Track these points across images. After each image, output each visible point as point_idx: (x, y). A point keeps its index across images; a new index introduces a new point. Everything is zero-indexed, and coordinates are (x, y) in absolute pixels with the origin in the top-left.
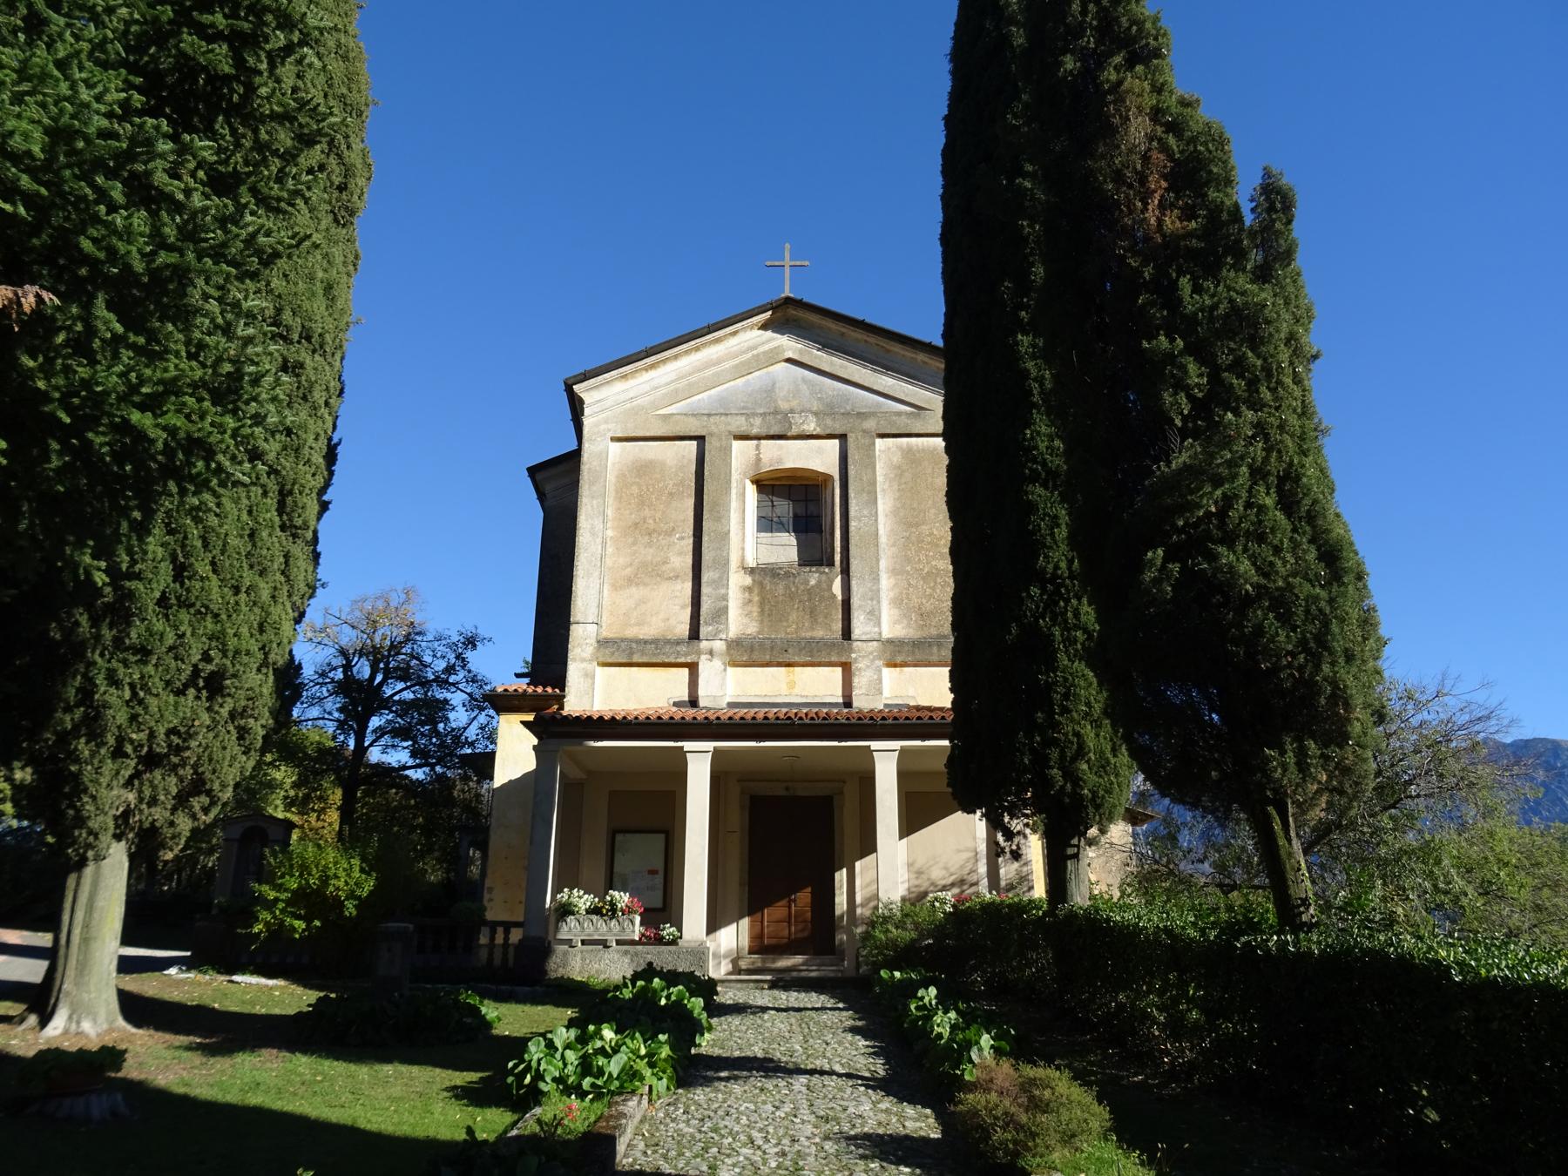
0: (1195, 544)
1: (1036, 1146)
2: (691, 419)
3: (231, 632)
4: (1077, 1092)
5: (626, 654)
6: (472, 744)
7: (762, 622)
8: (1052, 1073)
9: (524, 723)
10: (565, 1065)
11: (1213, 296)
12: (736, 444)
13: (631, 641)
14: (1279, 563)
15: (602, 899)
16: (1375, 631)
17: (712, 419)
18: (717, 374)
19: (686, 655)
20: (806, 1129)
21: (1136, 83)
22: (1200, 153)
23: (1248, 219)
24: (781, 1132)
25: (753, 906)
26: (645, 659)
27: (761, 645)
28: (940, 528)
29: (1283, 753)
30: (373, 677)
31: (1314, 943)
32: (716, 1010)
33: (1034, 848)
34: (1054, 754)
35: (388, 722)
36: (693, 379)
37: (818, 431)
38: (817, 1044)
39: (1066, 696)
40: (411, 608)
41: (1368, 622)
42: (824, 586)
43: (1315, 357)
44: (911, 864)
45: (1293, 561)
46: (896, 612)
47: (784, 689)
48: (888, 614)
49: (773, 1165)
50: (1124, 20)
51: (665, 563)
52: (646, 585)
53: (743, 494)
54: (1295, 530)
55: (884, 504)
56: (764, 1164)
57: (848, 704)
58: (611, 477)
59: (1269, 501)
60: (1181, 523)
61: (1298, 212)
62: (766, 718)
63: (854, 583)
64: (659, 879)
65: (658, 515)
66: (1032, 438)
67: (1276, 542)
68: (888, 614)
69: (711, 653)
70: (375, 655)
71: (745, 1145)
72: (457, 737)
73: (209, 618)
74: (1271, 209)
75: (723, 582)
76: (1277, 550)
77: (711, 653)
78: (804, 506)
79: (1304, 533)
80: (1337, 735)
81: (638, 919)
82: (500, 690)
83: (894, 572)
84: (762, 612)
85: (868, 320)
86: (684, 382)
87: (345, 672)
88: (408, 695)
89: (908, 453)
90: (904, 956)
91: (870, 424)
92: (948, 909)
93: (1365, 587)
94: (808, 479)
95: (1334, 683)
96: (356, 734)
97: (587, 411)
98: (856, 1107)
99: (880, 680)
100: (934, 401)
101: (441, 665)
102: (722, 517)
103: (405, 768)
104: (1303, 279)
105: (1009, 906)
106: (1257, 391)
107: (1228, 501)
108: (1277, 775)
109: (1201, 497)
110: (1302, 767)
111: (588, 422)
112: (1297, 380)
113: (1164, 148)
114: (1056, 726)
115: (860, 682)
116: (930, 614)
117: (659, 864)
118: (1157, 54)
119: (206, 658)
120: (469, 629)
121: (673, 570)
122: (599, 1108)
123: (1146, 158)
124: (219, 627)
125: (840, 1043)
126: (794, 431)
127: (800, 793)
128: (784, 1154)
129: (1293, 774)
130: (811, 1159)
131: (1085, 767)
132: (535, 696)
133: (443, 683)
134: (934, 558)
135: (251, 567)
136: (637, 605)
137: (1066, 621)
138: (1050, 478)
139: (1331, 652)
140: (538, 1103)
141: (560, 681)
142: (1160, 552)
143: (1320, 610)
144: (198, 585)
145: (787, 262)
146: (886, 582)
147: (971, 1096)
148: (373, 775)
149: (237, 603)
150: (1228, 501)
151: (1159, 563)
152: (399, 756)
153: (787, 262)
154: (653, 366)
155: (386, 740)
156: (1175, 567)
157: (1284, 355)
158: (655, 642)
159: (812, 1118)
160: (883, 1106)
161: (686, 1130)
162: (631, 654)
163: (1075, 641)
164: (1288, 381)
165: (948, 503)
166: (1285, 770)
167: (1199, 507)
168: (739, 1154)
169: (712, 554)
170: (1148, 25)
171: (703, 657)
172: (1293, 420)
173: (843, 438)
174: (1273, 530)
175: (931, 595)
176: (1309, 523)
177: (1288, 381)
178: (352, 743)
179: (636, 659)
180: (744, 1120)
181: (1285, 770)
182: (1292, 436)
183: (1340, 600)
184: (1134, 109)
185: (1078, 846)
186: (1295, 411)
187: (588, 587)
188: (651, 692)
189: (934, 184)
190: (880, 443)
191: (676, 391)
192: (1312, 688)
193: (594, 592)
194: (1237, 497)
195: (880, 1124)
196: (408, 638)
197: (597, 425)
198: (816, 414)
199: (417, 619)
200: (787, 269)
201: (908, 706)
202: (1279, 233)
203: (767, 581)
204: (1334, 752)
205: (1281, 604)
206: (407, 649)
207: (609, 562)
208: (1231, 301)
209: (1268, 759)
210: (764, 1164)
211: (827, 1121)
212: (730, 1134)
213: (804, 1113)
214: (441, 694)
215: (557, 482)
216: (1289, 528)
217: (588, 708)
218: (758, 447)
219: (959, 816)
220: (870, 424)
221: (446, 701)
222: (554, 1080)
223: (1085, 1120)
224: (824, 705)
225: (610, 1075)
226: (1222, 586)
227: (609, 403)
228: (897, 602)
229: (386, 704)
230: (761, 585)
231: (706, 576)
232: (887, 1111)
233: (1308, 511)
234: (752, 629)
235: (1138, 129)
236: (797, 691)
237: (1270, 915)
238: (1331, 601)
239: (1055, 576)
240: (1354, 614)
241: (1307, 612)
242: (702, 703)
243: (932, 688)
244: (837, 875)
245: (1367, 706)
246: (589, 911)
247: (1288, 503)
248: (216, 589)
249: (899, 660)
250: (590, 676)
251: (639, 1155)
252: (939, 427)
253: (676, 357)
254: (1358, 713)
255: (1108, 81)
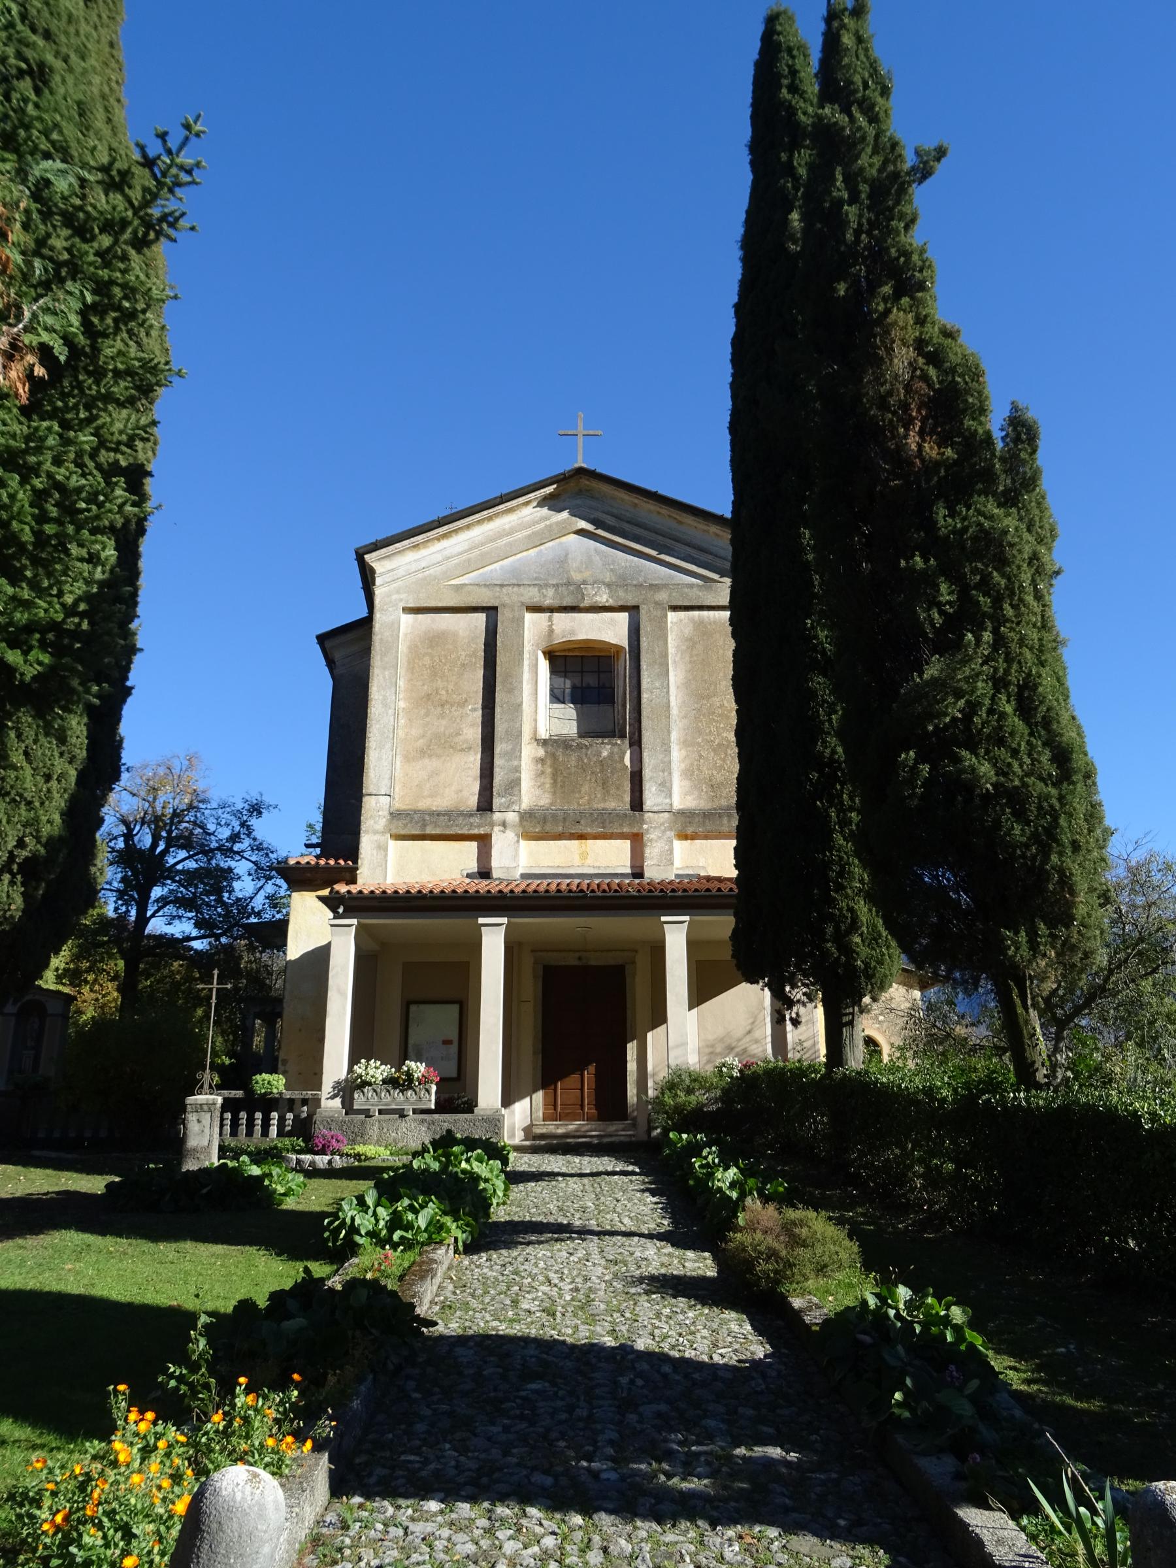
0: (939, 748)
1: (793, 1274)
2: (484, 590)
3: (45, 819)
4: (831, 1230)
5: (419, 827)
6: (258, 914)
7: (554, 793)
8: (811, 1214)
9: (320, 898)
10: (377, 1221)
11: (964, 519)
12: (528, 616)
13: (423, 812)
14: (1016, 765)
15: (399, 1070)
16: (1100, 822)
17: (504, 590)
18: (510, 544)
19: (479, 826)
20: (597, 1271)
21: (901, 317)
22: (958, 383)
23: (999, 445)
24: (575, 1273)
25: (547, 1079)
26: (438, 831)
27: (554, 816)
28: (727, 703)
29: (1017, 933)
30: (155, 845)
31: (1040, 1099)
32: (515, 1178)
33: (815, 1017)
34: (830, 929)
35: (171, 891)
36: (485, 549)
37: (611, 602)
38: (609, 1201)
39: (841, 874)
40: (192, 774)
41: (1094, 815)
42: (617, 757)
43: (1057, 573)
44: (701, 1034)
45: (1027, 764)
46: (687, 783)
47: (577, 861)
48: (678, 785)
49: (568, 1298)
50: (893, 251)
51: (458, 734)
52: (439, 756)
53: (536, 665)
54: (1031, 734)
55: (675, 676)
56: (560, 1298)
57: (638, 874)
58: (403, 648)
59: (1009, 709)
60: (931, 728)
61: (1042, 443)
62: (559, 891)
63: (645, 754)
64: (454, 1049)
65: (451, 687)
66: (813, 627)
67: (1014, 746)
68: (678, 785)
69: (504, 824)
70: (156, 822)
71: (542, 1284)
72: (242, 905)
73: (23, 806)
74: (1017, 440)
75: (515, 753)
76: (1015, 753)
77: (504, 824)
78: (597, 684)
79: (1040, 736)
80: (1062, 916)
81: (434, 1088)
82: (292, 862)
83: (685, 744)
84: (555, 782)
85: (661, 492)
86: (476, 552)
87: (126, 842)
88: (191, 865)
89: (700, 625)
90: (690, 1119)
91: (662, 596)
92: (736, 1074)
93: (1094, 784)
94: (600, 650)
95: (1061, 871)
96: (138, 904)
97: (378, 581)
98: (642, 1252)
99: (671, 851)
100: (722, 590)
101: (225, 833)
102: (515, 689)
103: (189, 938)
104: (1050, 501)
105: (790, 1070)
106: (1002, 609)
107: (972, 708)
108: (1010, 953)
109: (947, 707)
110: (1034, 946)
111: (379, 592)
112: (1038, 596)
113: (925, 378)
114: (832, 902)
115: (652, 853)
116: (720, 786)
117: (454, 1035)
118: (921, 287)
119: (21, 844)
120: (254, 797)
121: (466, 741)
122: (411, 1256)
123: (908, 387)
124: (32, 814)
125: (629, 1200)
126: (587, 603)
127: (593, 963)
128: (577, 1290)
129: (1025, 952)
130: (601, 1293)
131: (857, 940)
132: (327, 868)
133: (228, 852)
134: (724, 729)
135: (62, 754)
136: (430, 777)
137: (841, 803)
138: (825, 667)
139: (1059, 843)
140: (354, 1254)
141: (353, 853)
142: (912, 753)
143: (1051, 806)
144: (13, 774)
145: (581, 430)
146: (677, 754)
147: (739, 1235)
148: (155, 947)
149: (49, 791)
150: (972, 708)
151: (911, 763)
152: (183, 927)
153: (581, 430)
154: (445, 536)
155: (170, 909)
156: (925, 769)
157: (1026, 577)
158: (448, 814)
159: (603, 1262)
160: (665, 1251)
161: (490, 1274)
162: (424, 826)
163: (850, 823)
164: (1029, 599)
165: (735, 686)
166: (1017, 949)
167: (946, 714)
168: (537, 1291)
169: (505, 725)
170: (915, 257)
171: (496, 829)
172: (1034, 635)
173: (633, 610)
174: (1012, 734)
175: (721, 767)
176: (1044, 729)
177: (1029, 599)
178: (133, 913)
179: (429, 830)
180: (542, 1264)
181: (1017, 949)
182: (1031, 649)
183: (1069, 797)
184: (898, 342)
185: (853, 1014)
186: (1034, 625)
187: (380, 759)
188: (444, 866)
189: (724, 372)
190: (672, 616)
191: (469, 561)
192: (1042, 876)
193: (386, 763)
194: (980, 704)
195: (662, 1265)
196: (191, 807)
197: (389, 595)
198: (608, 585)
199: (200, 786)
200: (580, 439)
201: (699, 877)
202: (1024, 462)
203: (559, 753)
204: (1062, 932)
205: (1016, 799)
206: (190, 817)
207: (401, 733)
208: (980, 524)
209: (1005, 939)
210: (560, 1298)
211: (616, 1263)
212: (530, 1275)
213: (596, 1257)
214: (224, 863)
215: (348, 651)
216: (1026, 732)
217: (381, 881)
218: (550, 619)
219: (744, 986)
220: (662, 596)
221: (230, 870)
222: (369, 1234)
223: (837, 1253)
224: (616, 875)
225: (419, 1227)
226: (967, 785)
227: (401, 572)
228: (688, 773)
229: (170, 873)
230: (554, 756)
231: (499, 748)
232: (669, 1254)
233: (1044, 717)
234: (545, 800)
235: (902, 359)
236: (589, 862)
237: (1012, 1075)
238: (1061, 798)
239: (832, 760)
240: (1081, 809)
241: (1040, 808)
242: (495, 874)
243: (717, 859)
244: (629, 1046)
245: (1092, 890)
246: (384, 1081)
247: (1026, 709)
248: (29, 778)
249: (690, 830)
250: (383, 848)
251: (449, 1294)
252: (725, 600)
253: (468, 527)
254: (1081, 898)
255: (876, 311)
